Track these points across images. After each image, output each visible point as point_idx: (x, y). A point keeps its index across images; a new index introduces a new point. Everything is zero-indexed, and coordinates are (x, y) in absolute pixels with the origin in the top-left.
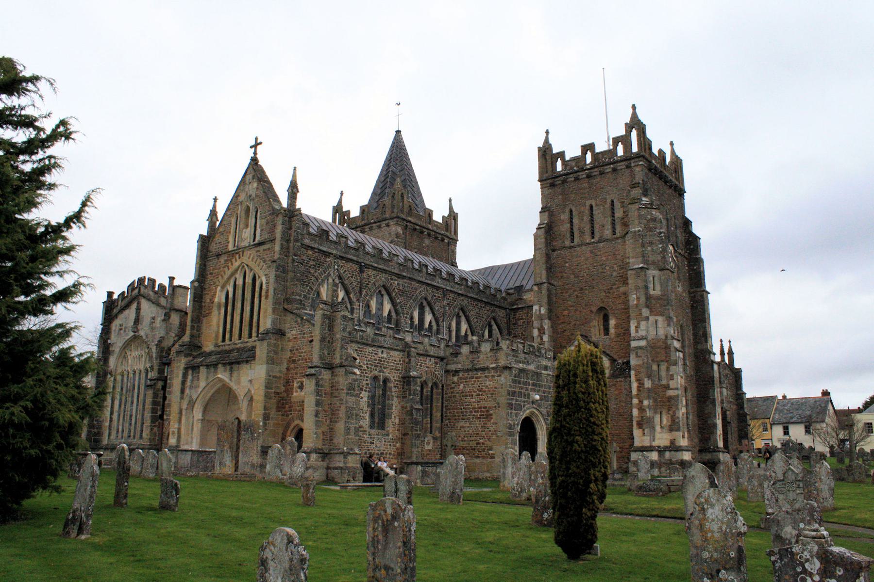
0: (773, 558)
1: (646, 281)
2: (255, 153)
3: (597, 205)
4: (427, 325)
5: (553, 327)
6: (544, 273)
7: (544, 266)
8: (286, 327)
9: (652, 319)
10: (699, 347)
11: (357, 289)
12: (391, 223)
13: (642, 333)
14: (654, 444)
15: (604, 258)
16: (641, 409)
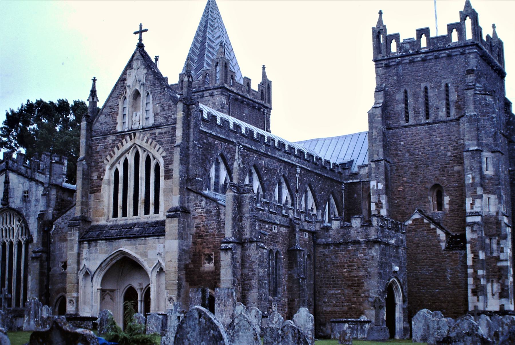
2: (140, 40)
3: (431, 88)
5: (389, 201)
6: (381, 150)
8: (191, 206)
9: (485, 196)
12: (215, 92)
13: (476, 209)
15: (438, 139)
16: (477, 279)
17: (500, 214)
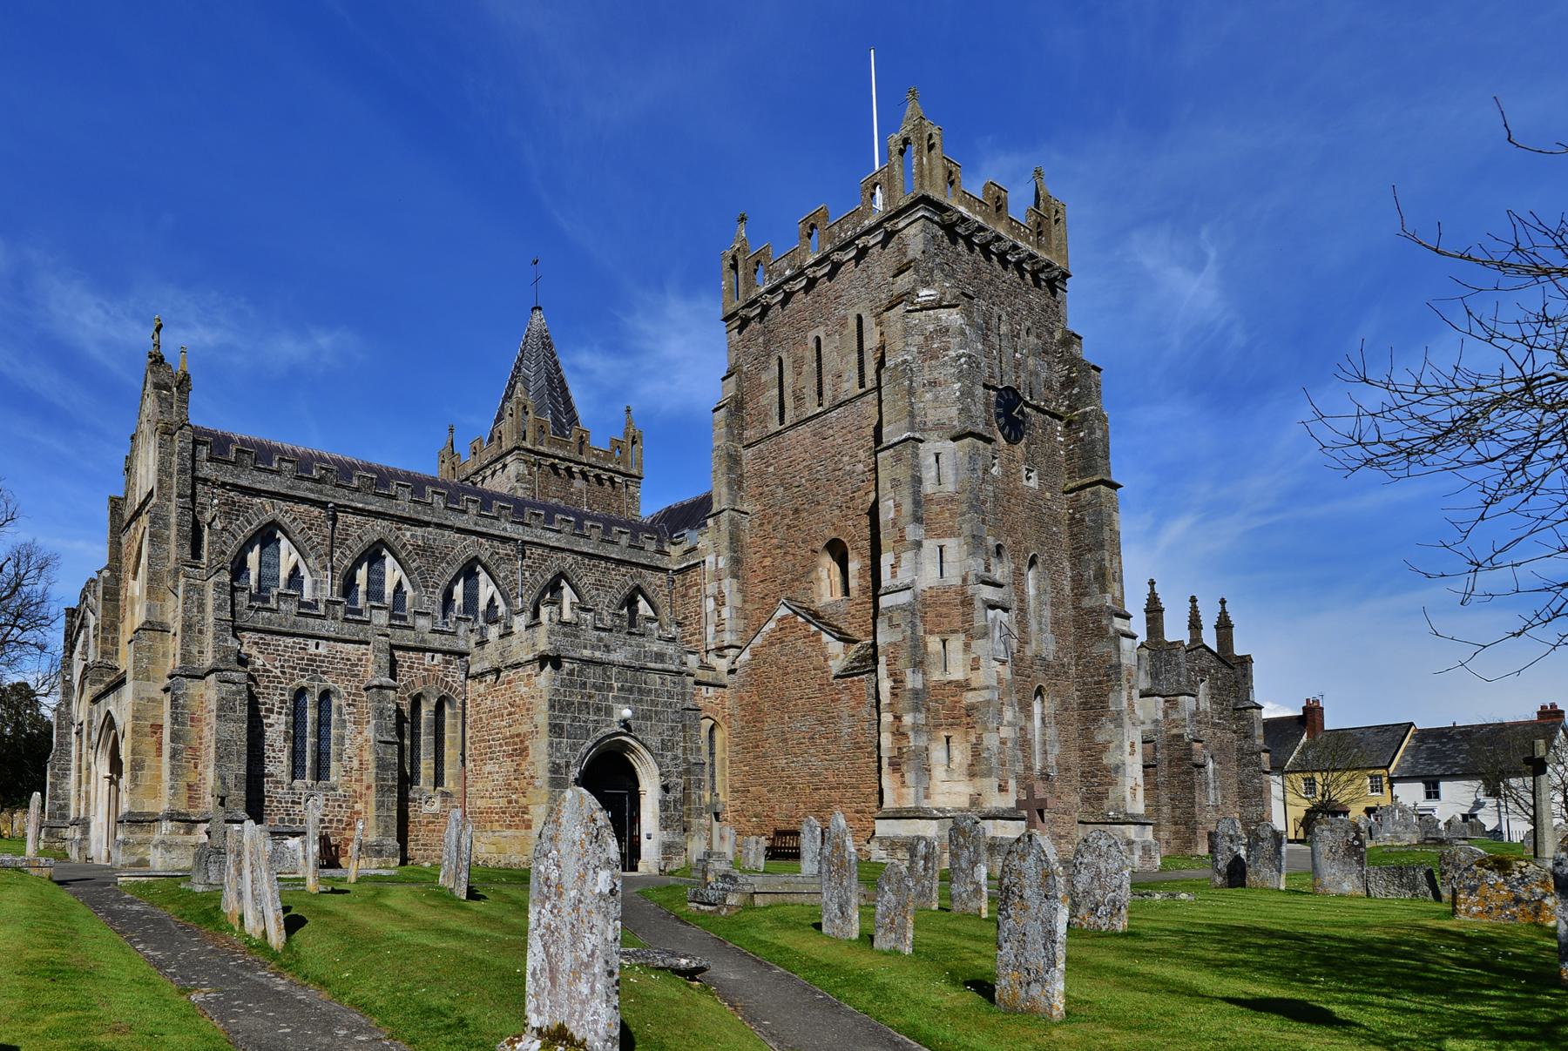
1: (916, 467)
7: (724, 479)
9: (930, 546)
10: (1087, 603)
11: (324, 549)
13: (904, 577)
14: (925, 804)
16: (899, 734)
17: (971, 578)
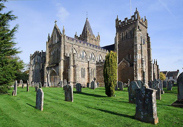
0: (136, 91)
4: (93, 58)
